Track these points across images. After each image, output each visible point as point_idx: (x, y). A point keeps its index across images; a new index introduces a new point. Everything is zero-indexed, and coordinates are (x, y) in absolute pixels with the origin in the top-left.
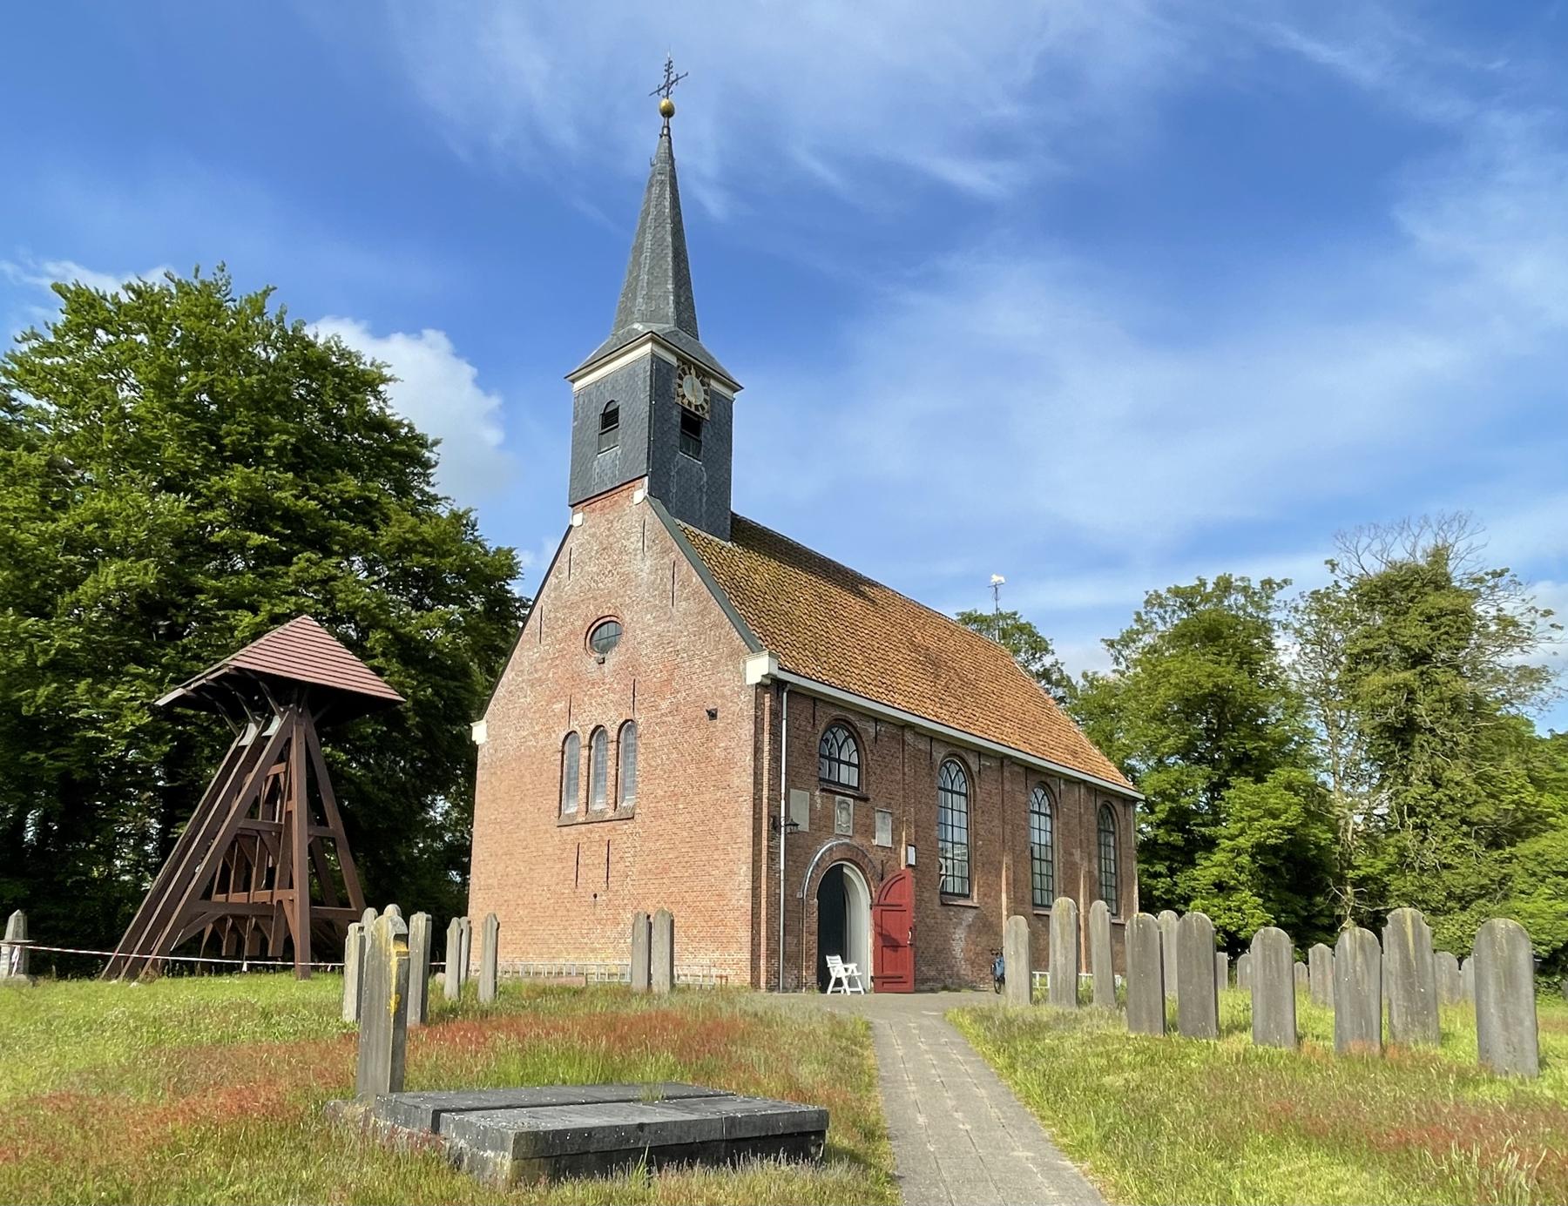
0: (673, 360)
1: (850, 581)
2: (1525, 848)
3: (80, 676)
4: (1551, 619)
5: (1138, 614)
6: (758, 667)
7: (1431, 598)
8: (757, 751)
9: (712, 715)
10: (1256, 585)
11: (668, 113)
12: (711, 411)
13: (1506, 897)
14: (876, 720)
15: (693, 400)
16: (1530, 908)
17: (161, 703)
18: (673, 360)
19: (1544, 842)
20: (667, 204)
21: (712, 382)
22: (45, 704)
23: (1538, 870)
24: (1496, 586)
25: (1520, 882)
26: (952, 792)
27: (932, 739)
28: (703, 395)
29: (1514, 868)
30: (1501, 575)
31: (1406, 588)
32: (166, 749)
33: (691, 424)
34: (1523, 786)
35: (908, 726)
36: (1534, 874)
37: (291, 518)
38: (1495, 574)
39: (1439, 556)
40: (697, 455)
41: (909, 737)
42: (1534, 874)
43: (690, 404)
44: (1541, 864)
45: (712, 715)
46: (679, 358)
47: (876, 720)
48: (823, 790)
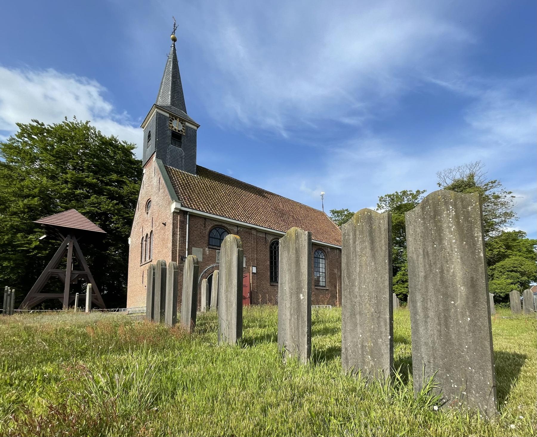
0: (168, 115)
1: (260, 192)
2: (498, 264)
3: (20, 231)
4: (511, 195)
5: (378, 204)
6: (174, 206)
7: (468, 190)
8: (174, 234)
9: (165, 224)
10: (415, 193)
11: (174, 40)
12: (186, 133)
13: (493, 279)
14: (237, 226)
15: (177, 128)
16: (498, 282)
17: (41, 238)
18: (168, 115)
19: (505, 262)
20: (171, 67)
21: (186, 123)
22: (6, 241)
23: (502, 270)
24: (492, 186)
25: (496, 275)
26: (215, 238)
27: (266, 233)
28: (182, 127)
29: (495, 272)
30: (495, 182)
31: (460, 187)
32: (47, 252)
33: (176, 137)
34: (501, 247)
35: (252, 228)
36: (501, 272)
37: (90, 186)
38: (492, 182)
39: (472, 176)
40: (180, 146)
41: (254, 232)
42: (501, 272)
43: (175, 129)
44: (503, 269)
45: (165, 224)
46: (170, 114)
47: (237, 226)
48: (209, 248)
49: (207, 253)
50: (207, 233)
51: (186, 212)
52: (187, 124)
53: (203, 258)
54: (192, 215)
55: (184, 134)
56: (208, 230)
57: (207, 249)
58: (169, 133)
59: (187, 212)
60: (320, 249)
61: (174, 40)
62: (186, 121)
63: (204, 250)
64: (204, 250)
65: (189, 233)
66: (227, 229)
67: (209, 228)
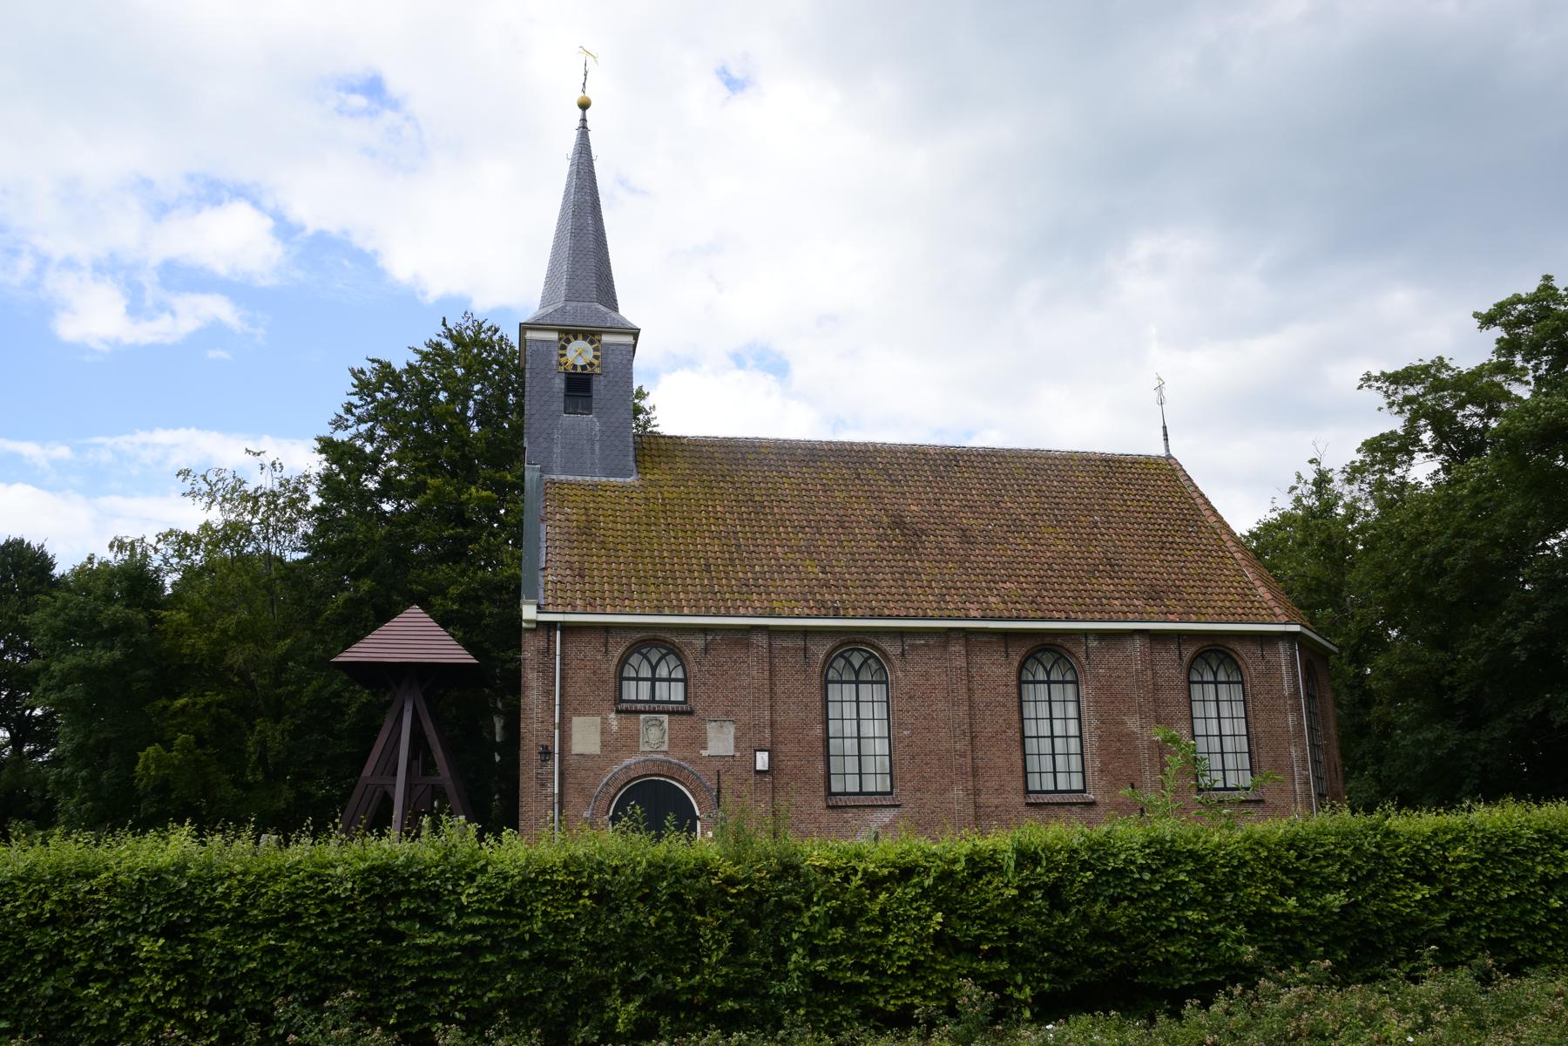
32: (117, 654)
46: (560, 331)
48: (618, 712)
49: (615, 728)
50: (612, 669)
51: (551, 626)
52: (606, 339)
53: (604, 745)
54: (567, 628)
55: (598, 371)
56: (616, 661)
57: (613, 715)
58: (559, 384)
59: (555, 623)
60: (1045, 649)
61: (584, 106)
62: (600, 333)
63: (605, 721)
64: (605, 721)
65: (562, 678)
66: (673, 644)
67: (617, 653)
